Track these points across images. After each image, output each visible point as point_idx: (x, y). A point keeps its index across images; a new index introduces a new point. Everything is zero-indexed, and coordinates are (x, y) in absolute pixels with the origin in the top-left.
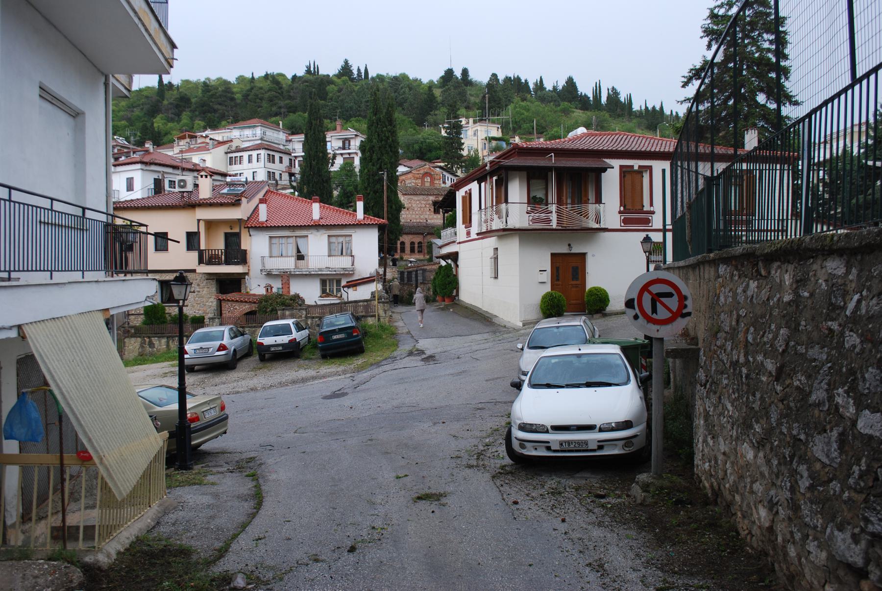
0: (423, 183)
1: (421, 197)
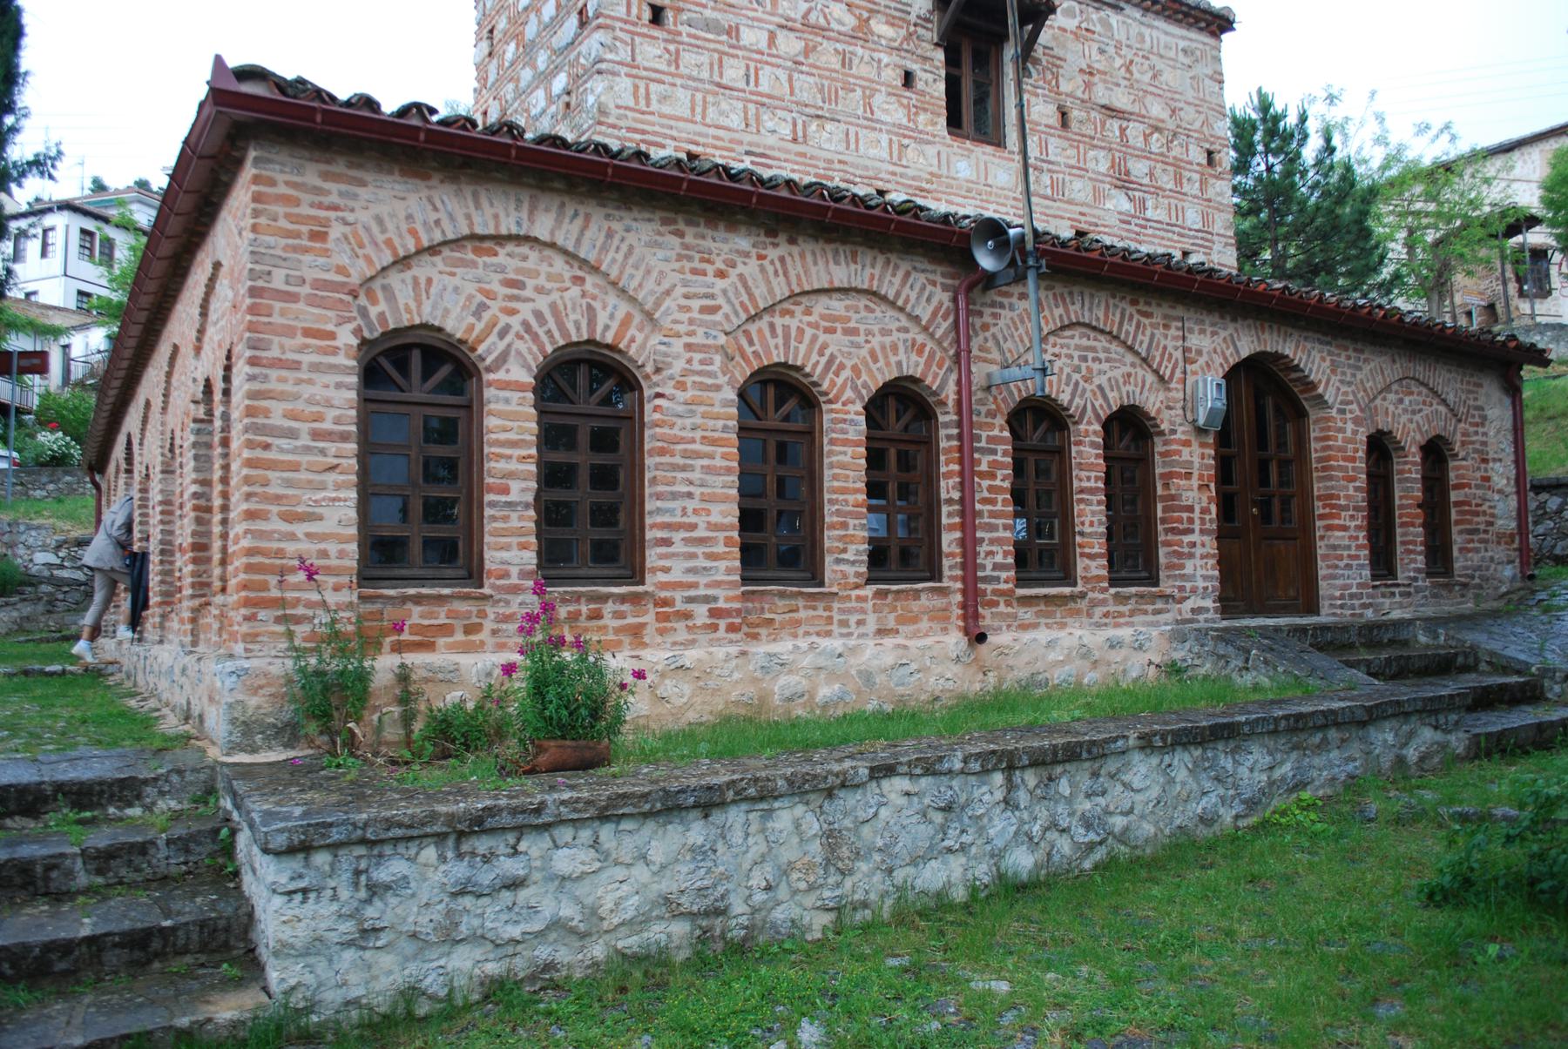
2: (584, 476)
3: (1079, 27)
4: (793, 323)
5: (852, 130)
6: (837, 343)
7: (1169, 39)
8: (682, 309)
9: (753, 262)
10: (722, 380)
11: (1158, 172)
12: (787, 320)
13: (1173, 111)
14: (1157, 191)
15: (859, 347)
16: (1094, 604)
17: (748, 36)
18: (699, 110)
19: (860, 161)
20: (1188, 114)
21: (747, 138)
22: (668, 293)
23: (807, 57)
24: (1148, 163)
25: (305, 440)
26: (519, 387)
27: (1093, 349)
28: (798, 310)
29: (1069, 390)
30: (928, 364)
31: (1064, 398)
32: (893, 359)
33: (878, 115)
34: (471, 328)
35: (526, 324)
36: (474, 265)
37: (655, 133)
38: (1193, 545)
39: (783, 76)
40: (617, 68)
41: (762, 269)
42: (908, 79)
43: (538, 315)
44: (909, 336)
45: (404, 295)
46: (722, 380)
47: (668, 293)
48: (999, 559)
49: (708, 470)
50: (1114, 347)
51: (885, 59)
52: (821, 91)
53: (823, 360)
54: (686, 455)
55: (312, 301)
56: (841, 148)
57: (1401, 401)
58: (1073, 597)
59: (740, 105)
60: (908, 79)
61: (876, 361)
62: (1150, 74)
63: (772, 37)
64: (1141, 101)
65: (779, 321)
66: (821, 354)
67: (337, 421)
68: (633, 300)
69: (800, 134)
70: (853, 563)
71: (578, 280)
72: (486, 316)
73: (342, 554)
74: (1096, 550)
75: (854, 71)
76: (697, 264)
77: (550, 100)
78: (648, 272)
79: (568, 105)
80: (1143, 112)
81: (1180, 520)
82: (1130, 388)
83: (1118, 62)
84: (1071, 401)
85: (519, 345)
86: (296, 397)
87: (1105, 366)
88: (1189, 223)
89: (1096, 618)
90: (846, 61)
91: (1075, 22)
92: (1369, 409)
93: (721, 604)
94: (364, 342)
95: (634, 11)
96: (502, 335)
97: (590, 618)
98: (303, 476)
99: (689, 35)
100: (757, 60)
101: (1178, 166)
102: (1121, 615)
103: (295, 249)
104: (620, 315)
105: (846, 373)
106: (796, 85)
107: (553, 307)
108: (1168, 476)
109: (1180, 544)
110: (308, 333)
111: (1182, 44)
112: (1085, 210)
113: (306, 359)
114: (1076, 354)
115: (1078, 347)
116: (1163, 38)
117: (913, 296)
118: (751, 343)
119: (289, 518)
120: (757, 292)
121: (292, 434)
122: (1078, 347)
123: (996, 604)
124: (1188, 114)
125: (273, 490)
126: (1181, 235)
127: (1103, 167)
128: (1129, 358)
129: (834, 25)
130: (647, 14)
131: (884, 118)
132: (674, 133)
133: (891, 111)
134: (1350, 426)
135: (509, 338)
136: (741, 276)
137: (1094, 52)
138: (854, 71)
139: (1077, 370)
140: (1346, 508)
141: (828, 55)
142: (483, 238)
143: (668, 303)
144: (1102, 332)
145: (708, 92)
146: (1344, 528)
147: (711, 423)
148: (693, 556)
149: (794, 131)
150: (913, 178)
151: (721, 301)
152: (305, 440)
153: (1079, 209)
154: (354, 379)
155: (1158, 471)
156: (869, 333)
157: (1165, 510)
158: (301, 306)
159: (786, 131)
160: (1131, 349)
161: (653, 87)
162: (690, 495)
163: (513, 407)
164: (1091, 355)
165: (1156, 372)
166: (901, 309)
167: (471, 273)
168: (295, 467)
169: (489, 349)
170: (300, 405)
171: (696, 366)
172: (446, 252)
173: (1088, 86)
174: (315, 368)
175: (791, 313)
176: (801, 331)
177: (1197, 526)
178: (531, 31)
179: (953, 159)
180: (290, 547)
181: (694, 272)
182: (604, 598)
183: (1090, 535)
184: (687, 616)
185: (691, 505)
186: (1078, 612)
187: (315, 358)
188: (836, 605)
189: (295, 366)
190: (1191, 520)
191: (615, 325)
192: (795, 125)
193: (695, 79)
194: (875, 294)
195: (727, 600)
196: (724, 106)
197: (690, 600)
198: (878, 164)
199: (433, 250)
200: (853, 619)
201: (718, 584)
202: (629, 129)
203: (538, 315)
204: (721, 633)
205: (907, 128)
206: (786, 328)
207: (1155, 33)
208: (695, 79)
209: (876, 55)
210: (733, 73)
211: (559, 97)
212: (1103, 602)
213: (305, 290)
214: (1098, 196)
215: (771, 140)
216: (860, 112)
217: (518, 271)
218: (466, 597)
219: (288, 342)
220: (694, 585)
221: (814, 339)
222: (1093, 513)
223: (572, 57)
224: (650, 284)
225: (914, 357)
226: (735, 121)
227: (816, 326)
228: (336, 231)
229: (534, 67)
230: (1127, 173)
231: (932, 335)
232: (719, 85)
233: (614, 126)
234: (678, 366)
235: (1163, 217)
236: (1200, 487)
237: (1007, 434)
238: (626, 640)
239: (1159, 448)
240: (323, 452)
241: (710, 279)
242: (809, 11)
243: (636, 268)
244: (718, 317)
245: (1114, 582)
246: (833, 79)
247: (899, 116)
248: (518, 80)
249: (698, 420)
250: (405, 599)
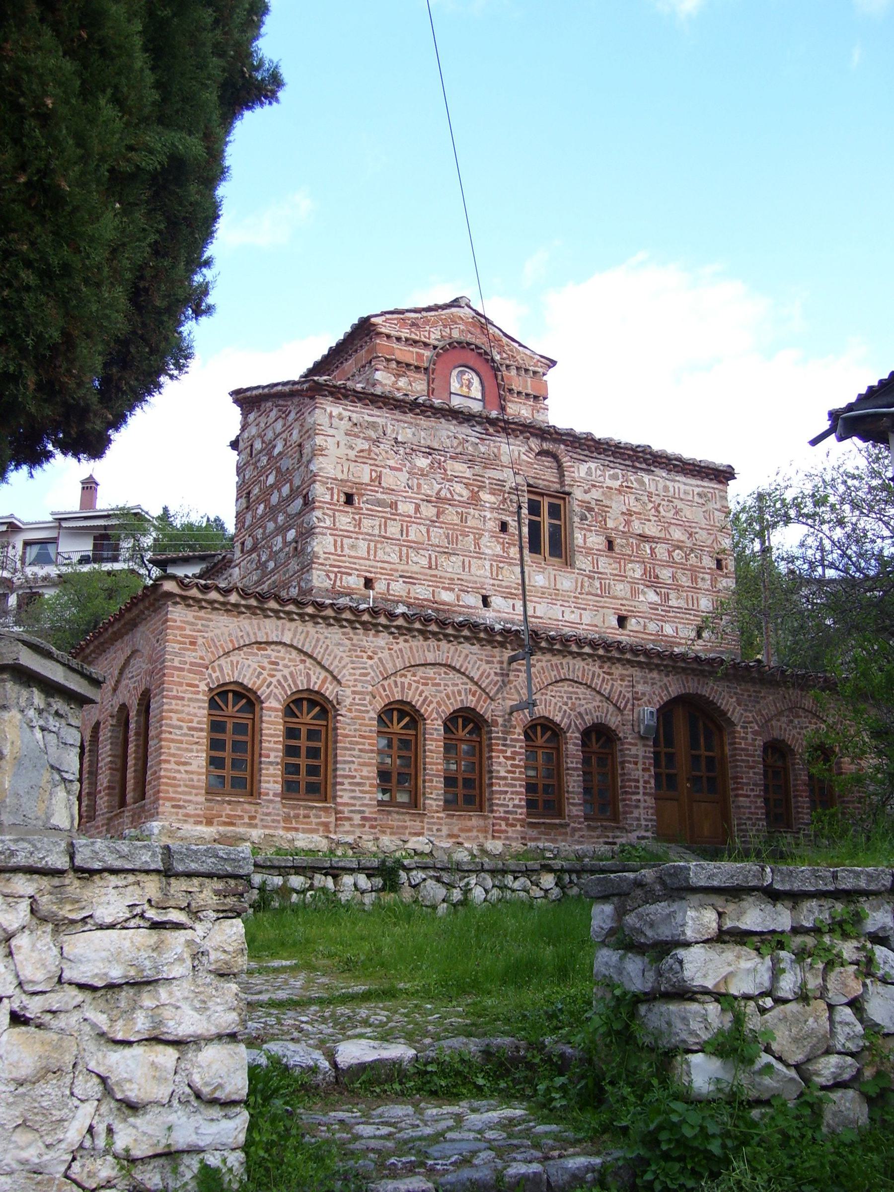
2: (303, 752)
3: (621, 486)
4: (406, 681)
5: (467, 559)
6: (429, 691)
7: (687, 487)
8: (350, 674)
9: (387, 652)
10: (369, 708)
11: (679, 574)
12: (403, 679)
13: (691, 535)
14: (678, 588)
15: (441, 692)
16: (574, 830)
17: (402, 508)
18: (372, 552)
19: (471, 578)
20: (702, 535)
21: (401, 567)
22: (344, 667)
23: (438, 517)
24: (671, 570)
25: (185, 731)
26: (276, 710)
27: (576, 693)
28: (409, 674)
29: (560, 715)
30: (478, 701)
31: (557, 719)
32: (459, 698)
33: (484, 550)
34: (255, 683)
35: (278, 681)
36: (257, 655)
37: (346, 567)
38: (639, 801)
39: (423, 529)
40: (325, 531)
41: (391, 655)
42: (504, 527)
43: (285, 677)
44: (468, 687)
45: (227, 670)
46: (369, 708)
47: (344, 667)
48: (516, 802)
49: (361, 750)
50: (588, 691)
51: (488, 515)
52: (447, 537)
53: (422, 699)
54: (351, 743)
55: (190, 671)
56: (460, 571)
57: (791, 721)
58: (561, 825)
59: (397, 548)
60: (504, 527)
61: (449, 699)
62: (673, 511)
63: (417, 508)
64: (666, 529)
65: (399, 680)
66: (420, 695)
67: (199, 723)
68: (327, 670)
69: (433, 563)
70: (435, 800)
71: (303, 661)
72: (261, 677)
73: (199, 780)
74: (577, 801)
75: (469, 524)
76: (359, 653)
77: (285, 543)
78: (335, 657)
79: (296, 548)
80: (668, 537)
81: (630, 787)
82: (598, 714)
83: (651, 505)
84: (562, 721)
85: (275, 690)
86: (182, 712)
87: (583, 702)
88: (702, 608)
89: (576, 838)
90: (463, 518)
91: (619, 483)
92: (766, 724)
93: (367, 815)
94: (211, 690)
95: (336, 497)
96: (268, 687)
97: (305, 817)
98: (184, 746)
99: (367, 509)
100: (407, 521)
101: (694, 572)
102: (592, 837)
103: (184, 649)
104: (321, 677)
105: (434, 705)
106: (432, 534)
107: (291, 674)
108: (623, 762)
109: (630, 800)
110: (189, 685)
111: (697, 490)
112: (624, 602)
113: (187, 696)
114: (565, 696)
115: (566, 692)
116: (682, 487)
117: (470, 666)
118: (385, 690)
119: (178, 763)
120: (387, 666)
121: (181, 728)
122: (566, 692)
123: (515, 826)
124: (702, 535)
125: (172, 751)
126: (695, 615)
127: (638, 574)
128: (598, 698)
129: (456, 497)
130: (343, 499)
131: (487, 551)
132: (357, 567)
133: (491, 547)
134: (750, 736)
135: (272, 687)
136: (380, 659)
137: (632, 500)
138: (469, 524)
139: (566, 704)
140: (748, 784)
141: (451, 515)
142: (261, 643)
143: (344, 671)
144: (581, 684)
145: (377, 542)
146: (748, 796)
147: (364, 728)
148: (353, 791)
149: (430, 562)
150: (506, 587)
151: (370, 670)
152: (185, 731)
153: (620, 602)
154: (207, 705)
155: (619, 760)
156: (446, 685)
157: (622, 781)
158: (185, 673)
159: (424, 562)
160: (599, 692)
161: (346, 541)
162: (353, 762)
163: (273, 719)
164: (574, 696)
165: (615, 705)
166: (463, 674)
167: (255, 659)
168: (181, 742)
169: (263, 692)
170: (184, 715)
171: (357, 701)
172: (245, 649)
173: (628, 523)
174: (190, 700)
175: (405, 676)
176: (410, 684)
177: (641, 790)
178: (274, 499)
179: (533, 574)
180: (178, 776)
181: (357, 657)
182: (312, 808)
183: (572, 792)
184: (350, 819)
185: (353, 767)
186: (566, 834)
187: (191, 696)
188: (426, 820)
189: (182, 699)
190: (637, 787)
191: (319, 682)
192: (430, 558)
193: (370, 535)
194: (449, 666)
195: (371, 813)
196: (388, 550)
197: (352, 812)
198: (483, 580)
199: (239, 649)
200: (435, 828)
201: (366, 805)
202: (331, 566)
203: (285, 677)
204: (367, 829)
205: (502, 557)
206: (403, 683)
207: (677, 485)
208: (370, 535)
209: (483, 513)
210: (393, 530)
211: (290, 543)
212: (580, 829)
213: (187, 666)
214: (634, 592)
215: (416, 568)
216: (472, 549)
217: (276, 657)
218: (250, 803)
219: (180, 689)
220: (354, 805)
221: (417, 688)
222: (575, 781)
223: (299, 521)
224: (336, 663)
225: (470, 697)
226: (394, 558)
227: (418, 682)
228: (200, 641)
229: (276, 522)
230: (657, 577)
231: (480, 687)
232: (384, 537)
233: (322, 564)
234: (348, 702)
235: (682, 604)
236: (644, 770)
237: (522, 737)
238: (321, 828)
239: (619, 747)
240: (193, 736)
241: (365, 660)
242: (441, 489)
243: (329, 655)
244: (368, 678)
245: (586, 819)
246: (454, 530)
247: (498, 550)
248: (265, 528)
249: (357, 727)
250: (224, 802)
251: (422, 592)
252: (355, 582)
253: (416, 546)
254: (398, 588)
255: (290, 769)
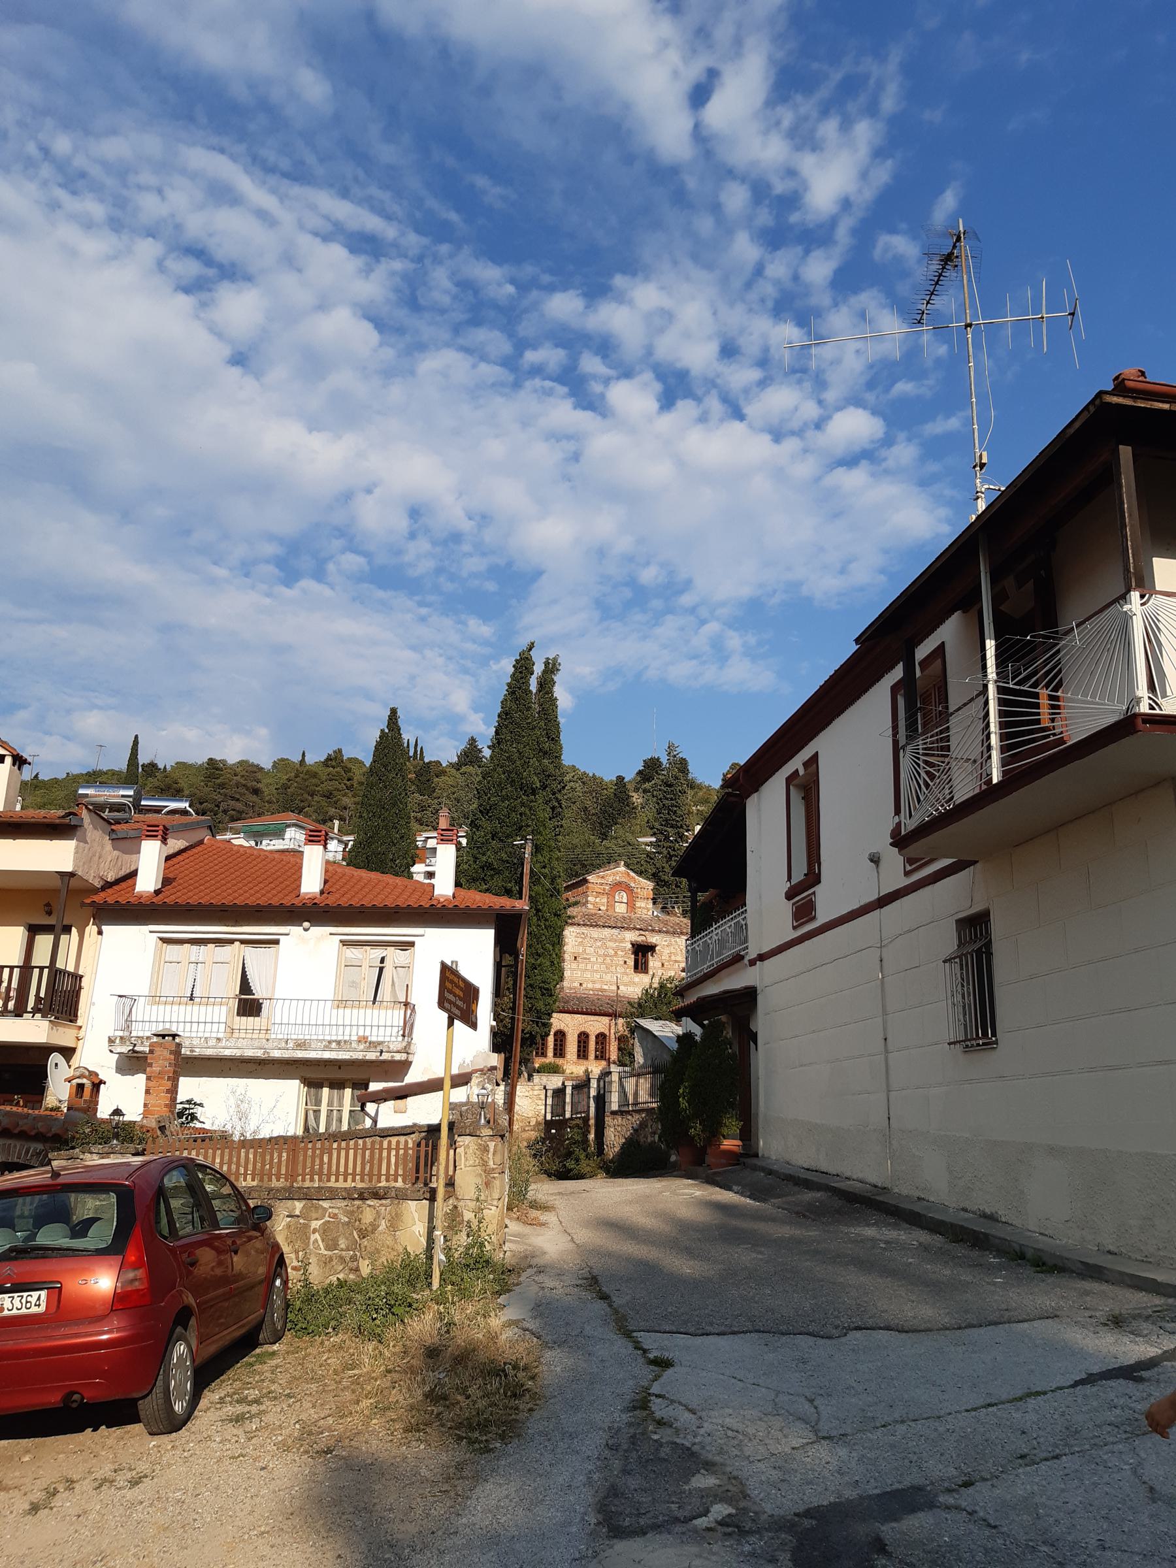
0: (611, 905)
1: (607, 932)
100: (594, 963)
251: (598, 986)
252: (576, 984)
253: (597, 971)
254: (590, 986)
255: (555, 1050)
